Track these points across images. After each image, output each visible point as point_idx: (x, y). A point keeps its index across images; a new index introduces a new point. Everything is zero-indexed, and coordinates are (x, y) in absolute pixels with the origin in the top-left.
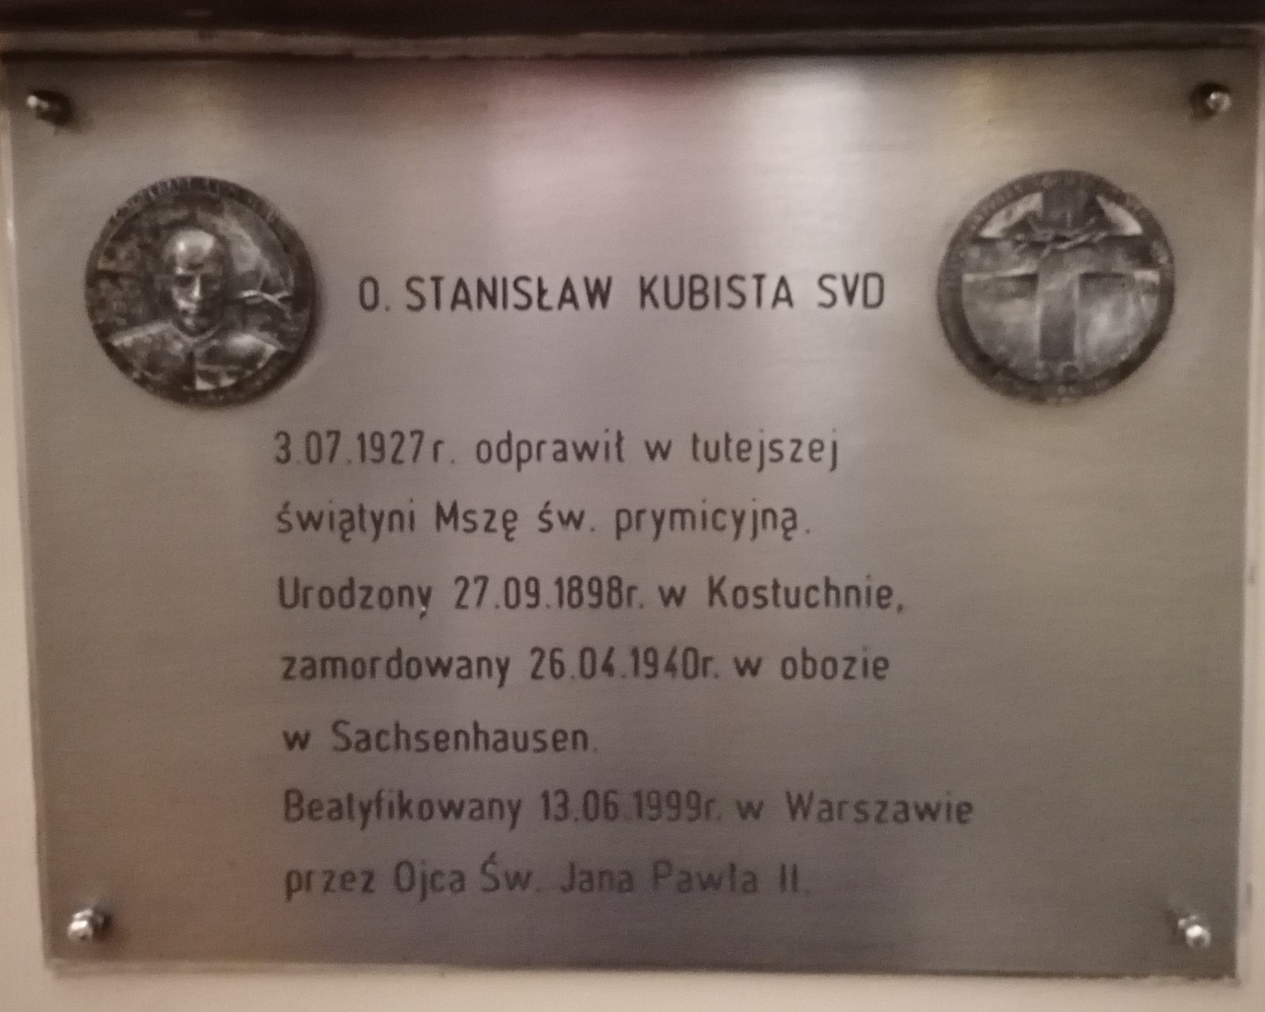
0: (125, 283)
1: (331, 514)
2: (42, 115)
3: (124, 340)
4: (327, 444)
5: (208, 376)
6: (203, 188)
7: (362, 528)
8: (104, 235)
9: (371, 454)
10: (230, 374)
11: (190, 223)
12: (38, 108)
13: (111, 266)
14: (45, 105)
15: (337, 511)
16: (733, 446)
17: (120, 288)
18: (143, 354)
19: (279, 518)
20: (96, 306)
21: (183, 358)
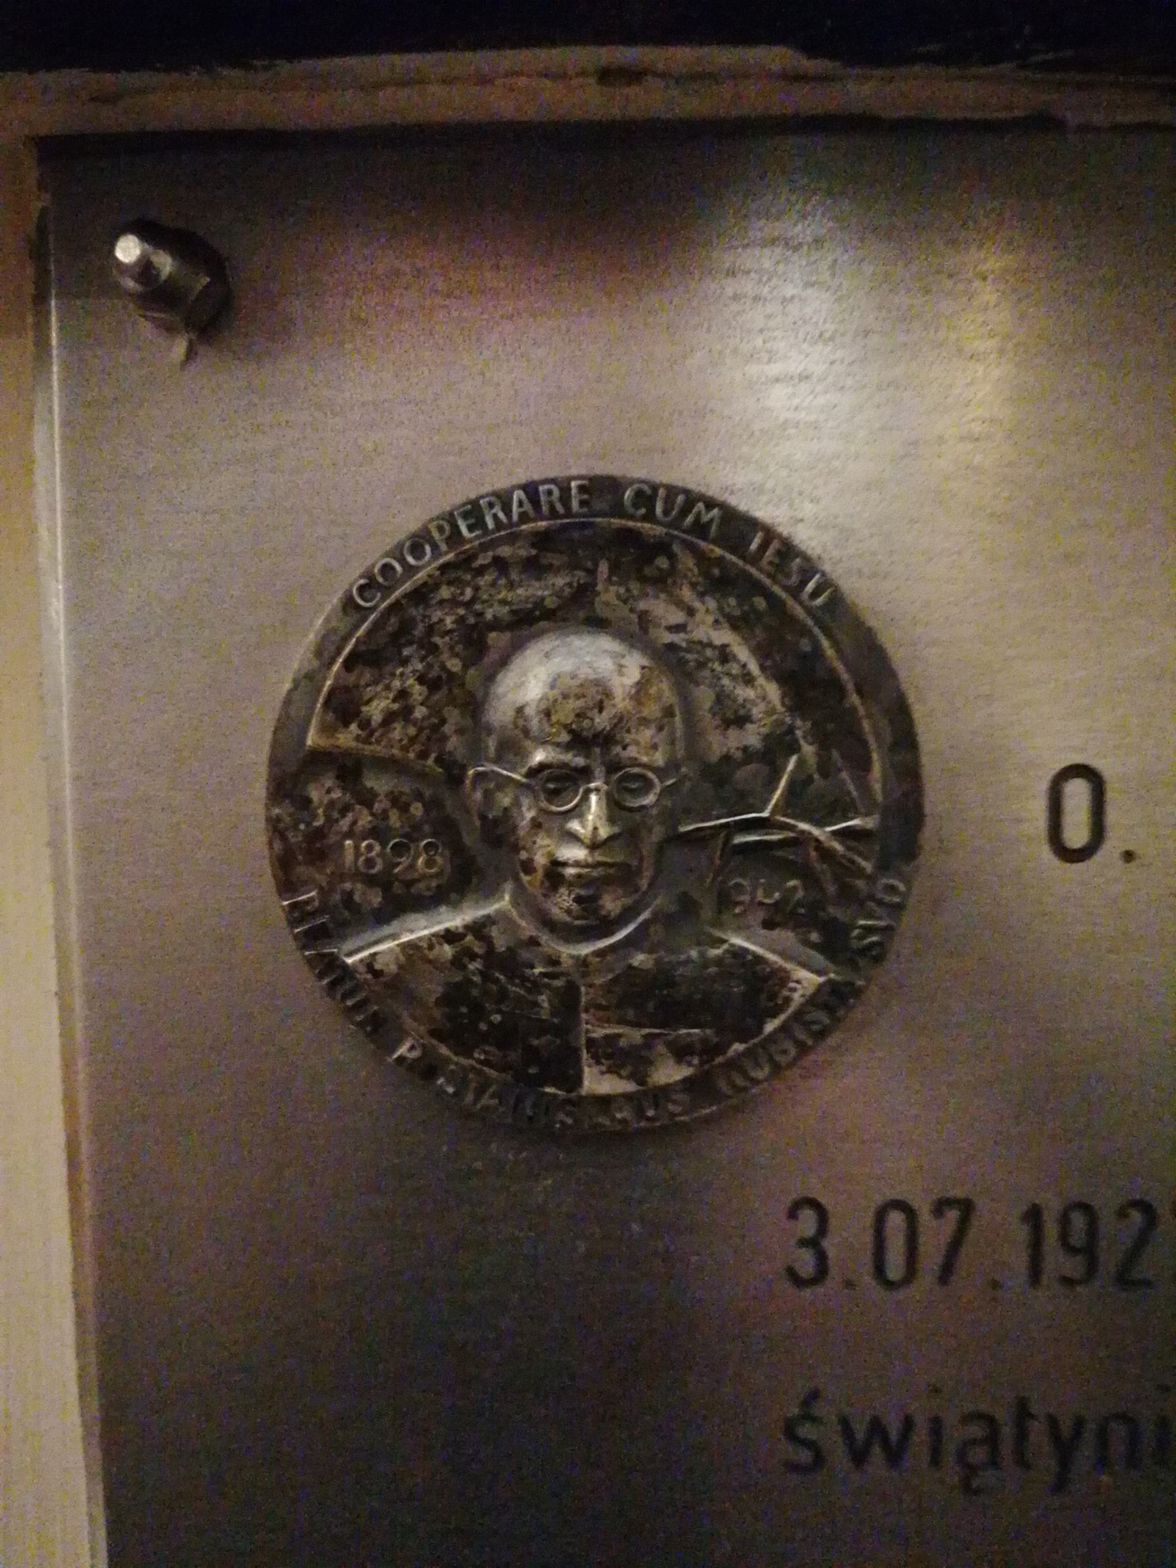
0: (379, 784)
1: (936, 1427)
2: (156, 295)
3: (381, 947)
4: (935, 1235)
5: (612, 1056)
6: (618, 510)
7: (1022, 1461)
8: (324, 653)
9: (1056, 1260)
10: (681, 1053)
11: (577, 612)
12: (144, 269)
13: (347, 738)
14: (165, 263)
15: (951, 1419)
16: (1038, 1431)
17: (367, 799)
18: (432, 988)
19: (790, 1432)
20: (297, 853)
21: (38, 388)
